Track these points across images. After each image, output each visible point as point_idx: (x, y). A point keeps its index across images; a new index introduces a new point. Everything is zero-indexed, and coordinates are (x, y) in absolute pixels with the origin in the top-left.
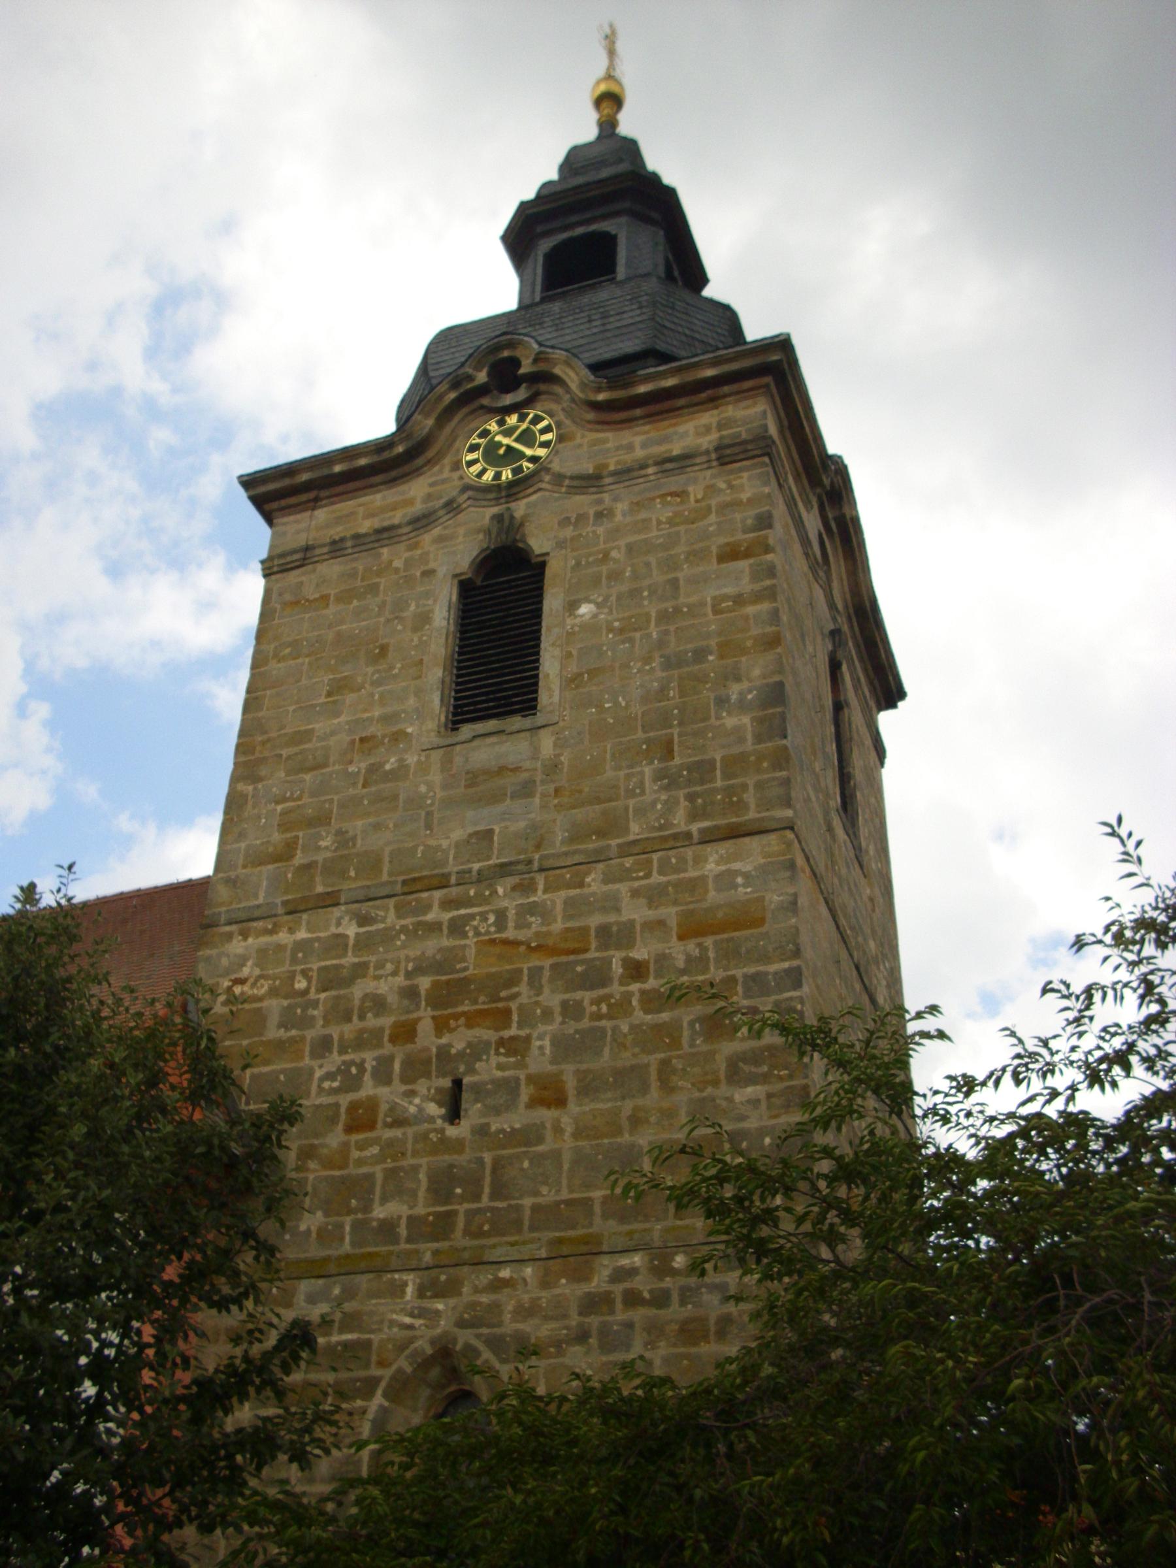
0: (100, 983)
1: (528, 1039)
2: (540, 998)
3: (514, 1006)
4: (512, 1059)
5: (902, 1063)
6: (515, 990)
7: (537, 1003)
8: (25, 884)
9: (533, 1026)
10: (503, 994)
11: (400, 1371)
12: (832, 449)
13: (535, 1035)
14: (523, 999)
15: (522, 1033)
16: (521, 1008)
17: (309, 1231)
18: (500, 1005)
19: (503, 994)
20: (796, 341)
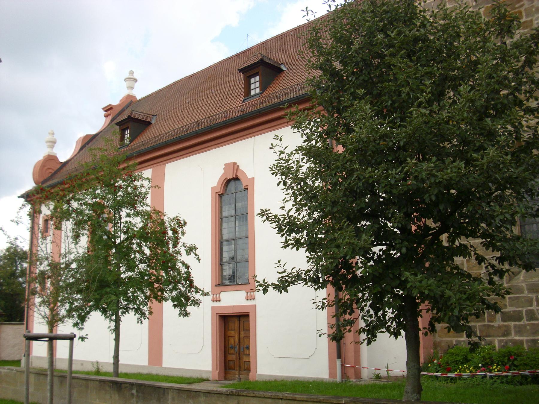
0: (370, 66)
1: (531, 21)
2: (534, 4)
3: (522, 9)
4: (526, 30)
5: (396, 378)
6: (522, 3)
7: (533, 7)
8: (25, 339)
9: (533, 16)
10: (517, 6)
11: (452, 341)
12: (223, 172)
13: (534, 19)
14: (526, 6)
15: (529, 19)
16: (525, 9)
17: (98, 294)
18: (516, 10)
19: (517, 6)
20: (226, 162)
